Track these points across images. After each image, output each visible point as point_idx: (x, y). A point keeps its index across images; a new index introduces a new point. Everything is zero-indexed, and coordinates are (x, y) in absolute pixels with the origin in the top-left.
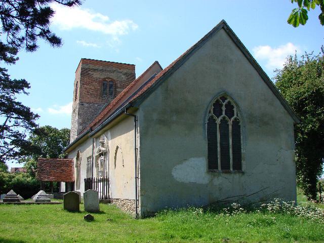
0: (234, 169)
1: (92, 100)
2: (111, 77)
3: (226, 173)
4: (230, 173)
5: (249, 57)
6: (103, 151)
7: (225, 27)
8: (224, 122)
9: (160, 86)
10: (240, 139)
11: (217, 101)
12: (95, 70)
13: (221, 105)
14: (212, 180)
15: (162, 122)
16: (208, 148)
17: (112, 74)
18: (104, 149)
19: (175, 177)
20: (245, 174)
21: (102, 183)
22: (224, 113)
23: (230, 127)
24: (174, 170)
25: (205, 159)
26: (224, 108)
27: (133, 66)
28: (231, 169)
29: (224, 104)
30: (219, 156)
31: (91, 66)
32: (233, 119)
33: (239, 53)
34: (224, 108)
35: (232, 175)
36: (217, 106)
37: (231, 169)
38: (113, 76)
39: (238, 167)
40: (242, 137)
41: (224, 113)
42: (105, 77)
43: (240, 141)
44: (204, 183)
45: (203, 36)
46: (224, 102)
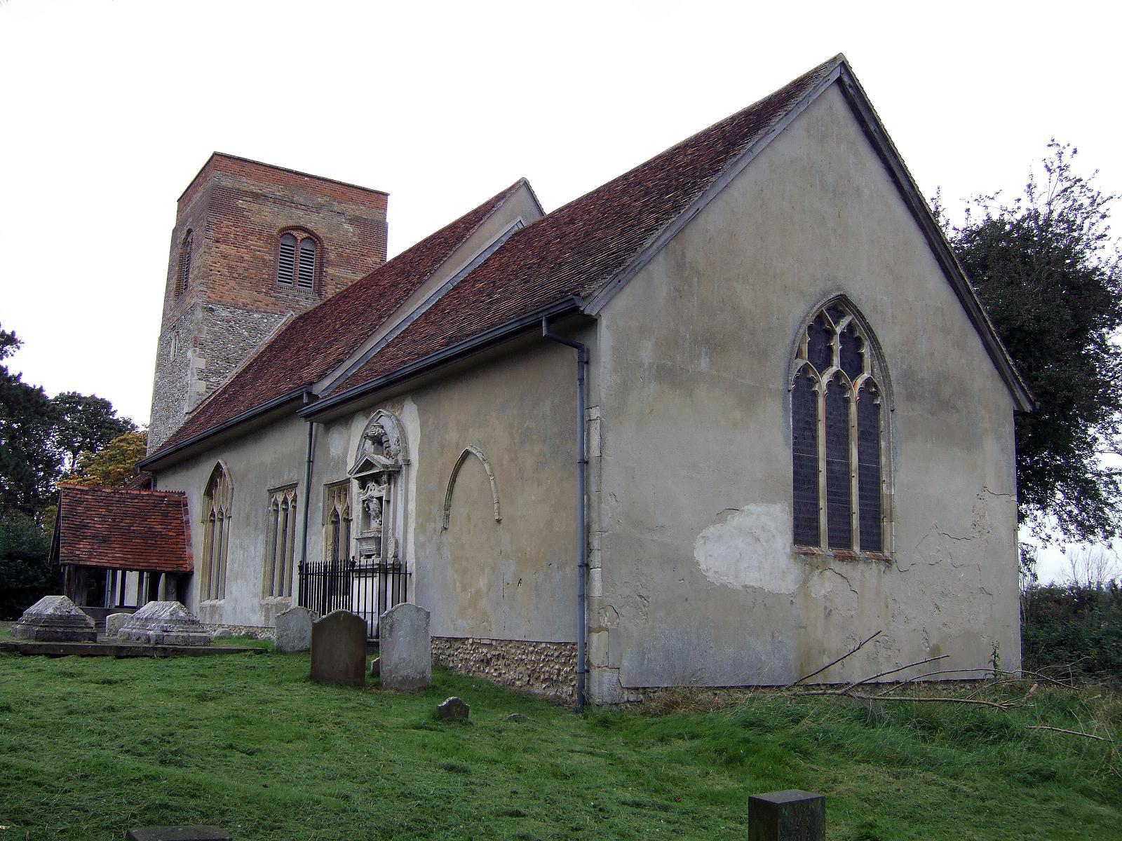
0: (863, 548)
1: (245, 296)
2: (309, 226)
3: (843, 559)
4: (852, 559)
5: (906, 187)
6: (385, 466)
7: (846, 79)
8: (837, 386)
9: (662, 254)
10: (878, 449)
11: (820, 318)
12: (256, 196)
13: (830, 333)
14: (805, 581)
15: (668, 375)
16: (795, 473)
17: (315, 216)
18: (383, 460)
19: (703, 567)
20: (894, 566)
21: (376, 580)
22: (836, 360)
23: (853, 408)
24: (700, 542)
25: (786, 504)
26: (836, 344)
27: (378, 199)
28: (856, 548)
29: (838, 330)
30: (823, 503)
31: (248, 184)
32: (860, 381)
33: (873, 166)
34: (836, 344)
35: (861, 566)
36: (819, 329)
37: (856, 548)
38: (314, 222)
39: (873, 541)
40: (883, 444)
41: (836, 360)
42: (291, 223)
43: (878, 457)
44: (783, 591)
45: (199, 171)
46: (837, 323)
